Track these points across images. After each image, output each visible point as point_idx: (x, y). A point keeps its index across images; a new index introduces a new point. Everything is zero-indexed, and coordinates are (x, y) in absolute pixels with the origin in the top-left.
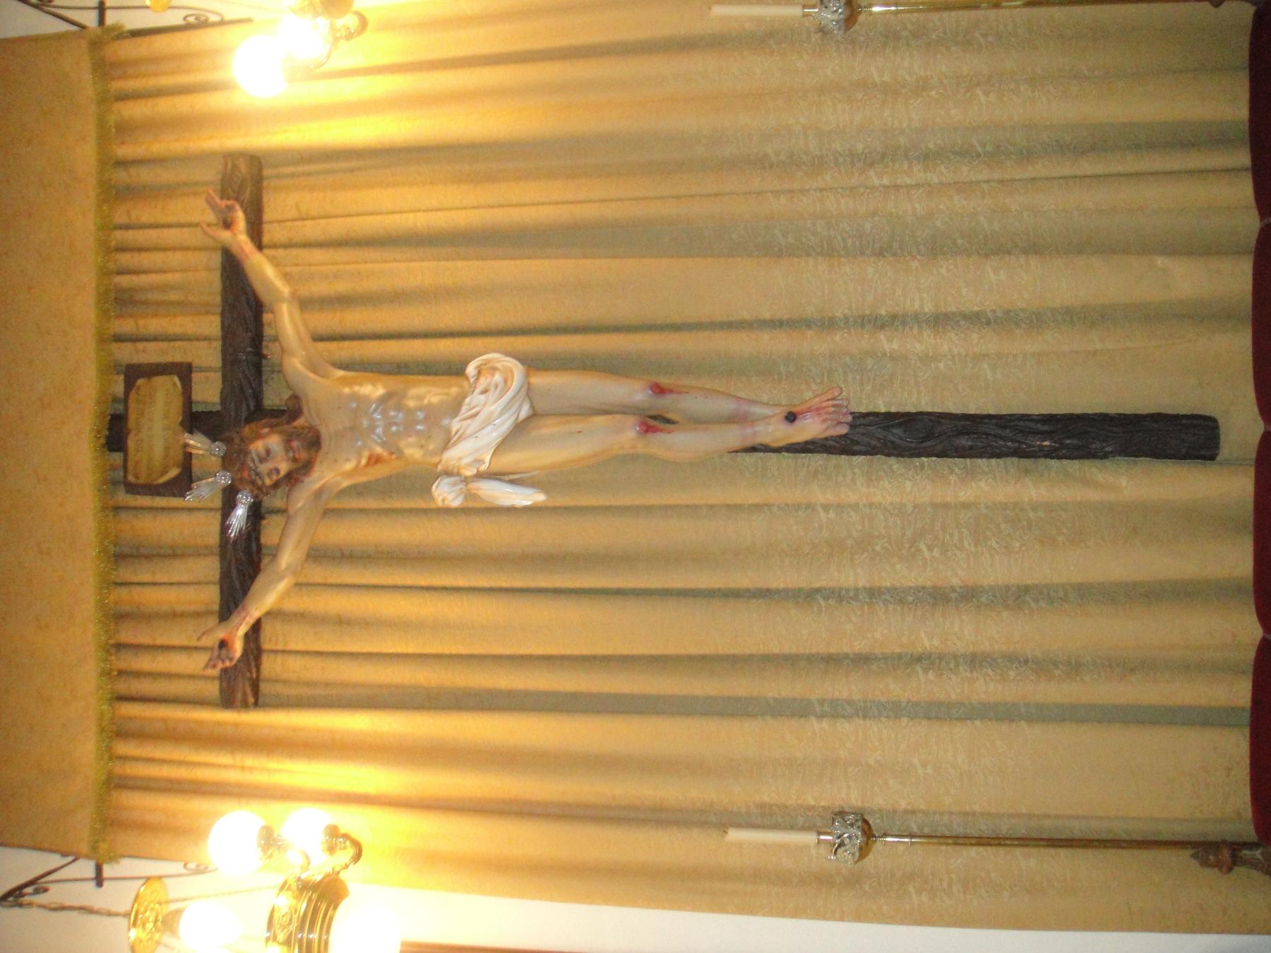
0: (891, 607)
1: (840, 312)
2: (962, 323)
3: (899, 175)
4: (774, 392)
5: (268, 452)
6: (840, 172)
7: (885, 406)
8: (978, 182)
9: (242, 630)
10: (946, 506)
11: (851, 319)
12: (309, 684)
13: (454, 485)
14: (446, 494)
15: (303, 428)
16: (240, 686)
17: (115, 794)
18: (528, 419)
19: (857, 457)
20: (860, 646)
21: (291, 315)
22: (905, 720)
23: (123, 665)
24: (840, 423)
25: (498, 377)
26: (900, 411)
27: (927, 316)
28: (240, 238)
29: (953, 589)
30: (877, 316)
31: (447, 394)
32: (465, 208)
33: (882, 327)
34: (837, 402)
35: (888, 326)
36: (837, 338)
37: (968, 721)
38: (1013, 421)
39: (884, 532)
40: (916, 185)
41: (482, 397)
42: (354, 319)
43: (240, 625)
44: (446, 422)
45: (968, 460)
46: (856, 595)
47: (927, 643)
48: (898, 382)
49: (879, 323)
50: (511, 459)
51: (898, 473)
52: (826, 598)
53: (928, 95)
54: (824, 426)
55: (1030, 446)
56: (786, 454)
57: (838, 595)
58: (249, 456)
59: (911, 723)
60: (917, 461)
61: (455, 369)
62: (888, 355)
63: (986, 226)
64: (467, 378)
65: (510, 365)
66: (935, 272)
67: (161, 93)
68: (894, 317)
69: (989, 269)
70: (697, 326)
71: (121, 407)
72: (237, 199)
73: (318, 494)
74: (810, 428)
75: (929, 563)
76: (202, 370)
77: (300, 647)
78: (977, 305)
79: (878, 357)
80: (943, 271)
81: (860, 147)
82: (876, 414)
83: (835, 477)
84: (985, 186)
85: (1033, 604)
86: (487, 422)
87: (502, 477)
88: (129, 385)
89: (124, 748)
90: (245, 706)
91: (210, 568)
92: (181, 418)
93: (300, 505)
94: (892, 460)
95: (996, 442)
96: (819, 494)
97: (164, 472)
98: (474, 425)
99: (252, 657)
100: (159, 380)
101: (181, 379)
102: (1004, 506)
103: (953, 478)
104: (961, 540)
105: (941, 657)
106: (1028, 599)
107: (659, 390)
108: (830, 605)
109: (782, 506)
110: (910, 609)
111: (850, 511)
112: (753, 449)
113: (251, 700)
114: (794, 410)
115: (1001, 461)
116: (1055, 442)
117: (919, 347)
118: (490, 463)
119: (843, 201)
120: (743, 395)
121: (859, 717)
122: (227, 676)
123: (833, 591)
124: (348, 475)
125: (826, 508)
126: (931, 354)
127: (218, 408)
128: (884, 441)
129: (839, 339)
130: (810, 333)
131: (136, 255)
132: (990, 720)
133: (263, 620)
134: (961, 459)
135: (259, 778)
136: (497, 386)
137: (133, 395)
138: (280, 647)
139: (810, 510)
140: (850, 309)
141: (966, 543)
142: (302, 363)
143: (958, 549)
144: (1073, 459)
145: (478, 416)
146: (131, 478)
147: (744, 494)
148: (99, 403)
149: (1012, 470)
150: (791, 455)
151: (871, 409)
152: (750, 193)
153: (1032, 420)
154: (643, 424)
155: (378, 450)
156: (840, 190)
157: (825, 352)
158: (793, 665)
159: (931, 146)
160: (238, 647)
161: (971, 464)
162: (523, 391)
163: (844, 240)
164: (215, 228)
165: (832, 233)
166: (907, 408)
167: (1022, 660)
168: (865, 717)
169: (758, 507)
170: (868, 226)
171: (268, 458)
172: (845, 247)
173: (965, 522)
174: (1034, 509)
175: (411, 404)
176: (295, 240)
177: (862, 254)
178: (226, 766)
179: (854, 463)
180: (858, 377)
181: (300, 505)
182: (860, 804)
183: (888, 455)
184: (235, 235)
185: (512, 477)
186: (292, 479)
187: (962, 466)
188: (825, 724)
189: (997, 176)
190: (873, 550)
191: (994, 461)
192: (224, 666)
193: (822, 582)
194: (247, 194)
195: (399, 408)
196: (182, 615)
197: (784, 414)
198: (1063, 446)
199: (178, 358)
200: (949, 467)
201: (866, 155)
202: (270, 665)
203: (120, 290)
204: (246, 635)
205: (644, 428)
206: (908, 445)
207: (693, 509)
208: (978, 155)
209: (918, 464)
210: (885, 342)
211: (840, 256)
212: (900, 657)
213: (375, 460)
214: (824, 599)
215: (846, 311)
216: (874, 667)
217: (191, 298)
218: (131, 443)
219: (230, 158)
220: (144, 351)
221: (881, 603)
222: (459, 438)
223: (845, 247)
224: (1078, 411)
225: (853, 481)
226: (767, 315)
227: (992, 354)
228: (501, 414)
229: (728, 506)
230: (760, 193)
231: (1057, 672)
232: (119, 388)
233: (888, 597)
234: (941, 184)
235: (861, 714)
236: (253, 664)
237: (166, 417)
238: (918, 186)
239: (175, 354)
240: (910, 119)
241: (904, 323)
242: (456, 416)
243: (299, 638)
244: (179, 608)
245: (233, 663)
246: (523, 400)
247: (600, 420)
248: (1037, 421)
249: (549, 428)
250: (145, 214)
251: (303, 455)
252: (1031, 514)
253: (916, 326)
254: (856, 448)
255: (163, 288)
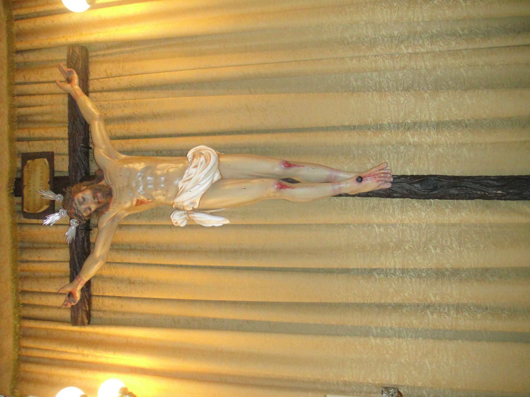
0: (413, 279)
1: (386, 121)
2: (452, 126)
3: (417, 47)
4: (351, 164)
5: (84, 199)
6: (385, 46)
7: (410, 171)
8: (461, 50)
9: (80, 287)
10: (443, 225)
11: (392, 125)
12: (115, 312)
13: (181, 215)
14: (178, 219)
15: (103, 186)
16: (80, 315)
17: (22, 366)
18: (219, 181)
19: (395, 199)
20: (397, 300)
21: (99, 125)
22: (421, 339)
23: (26, 302)
24: (386, 182)
25: (202, 159)
26: (419, 174)
27: (433, 123)
28: (76, 88)
29: (447, 270)
30: (405, 123)
31: (177, 168)
32: (189, 70)
33: (409, 129)
34: (385, 171)
35: (412, 129)
36: (384, 135)
37: (455, 341)
38: (481, 180)
39: (410, 239)
40: (426, 52)
41: (194, 170)
42: (134, 128)
43: (78, 285)
44: (176, 182)
45: (455, 201)
46: (395, 272)
47: (433, 299)
48: (417, 159)
49: (407, 127)
50: (211, 202)
51: (417, 208)
52: (379, 274)
53: (433, 3)
54: (377, 184)
55: (489, 193)
56: (357, 198)
57: (385, 273)
58: (74, 202)
59: (424, 341)
60: (428, 201)
61: (182, 154)
62: (412, 144)
63: (464, 74)
64: (187, 159)
65: (209, 152)
66: (438, 99)
67: (39, 15)
68: (415, 123)
69: (467, 97)
70: (310, 130)
71: (19, 176)
72: (74, 69)
73: (113, 219)
74: (370, 185)
75: (434, 256)
76: (59, 154)
77: (111, 294)
78: (460, 117)
79: (406, 145)
80: (442, 99)
81: (396, 33)
82: (406, 176)
83: (384, 210)
84: (465, 52)
85: (490, 278)
86: (197, 183)
87: (207, 212)
88: (24, 163)
89: (26, 343)
90: (83, 324)
91: (65, 254)
92: (48, 180)
93: (104, 224)
94: (414, 201)
95: (471, 191)
96: (375, 218)
97: (41, 207)
98: (189, 185)
99: (86, 300)
100: (37, 160)
101: (48, 160)
102: (475, 225)
103: (447, 211)
104: (451, 244)
105: (440, 305)
106: (488, 275)
107: (288, 165)
108: (381, 278)
109: (355, 225)
110: (424, 281)
111: (392, 227)
112: (340, 195)
113: (86, 321)
114: (362, 175)
115: (474, 201)
116: (504, 192)
117: (429, 140)
118: (199, 205)
119: (387, 61)
120: (334, 166)
121: (396, 337)
122: (74, 309)
123: (382, 270)
124: (128, 210)
125: (379, 226)
126: (435, 144)
127: (67, 175)
128: (410, 191)
129: (385, 136)
130: (369, 133)
131: (28, 97)
132: (467, 339)
133: (92, 281)
134: (452, 200)
135: (91, 359)
136: (201, 164)
137: (25, 169)
138: (101, 294)
139: (370, 227)
140: (392, 120)
141: (454, 245)
142: (104, 153)
143: (450, 248)
144: (513, 200)
145: (192, 180)
146: (25, 210)
147: (335, 218)
148: (11, 172)
149: (479, 207)
150: (360, 198)
151: (402, 173)
152: (337, 58)
153: (491, 180)
154: (279, 183)
155: (142, 198)
156: (385, 56)
157: (378, 143)
158: (361, 308)
159: (434, 31)
160: (78, 295)
161: (457, 202)
162: (216, 167)
163: (388, 83)
164: (63, 83)
165: (381, 79)
166: (422, 173)
167: (484, 307)
168: (399, 337)
169: (343, 225)
170: (400, 75)
171: (84, 203)
172: (388, 87)
173: (454, 234)
174: (491, 227)
175: (159, 172)
176: (105, 88)
177: (398, 90)
178: (75, 354)
179: (394, 203)
180: (396, 156)
181: (104, 224)
182: (396, 383)
183: (412, 198)
184: (72, 86)
185: (211, 211)
186: (99, 212)
187: (452, 204)
188: (378, 341)
189: (470, 47)
190: (404, 249)
191: (469, 201)
192: (71, 305)
193: (377, 265)
194: (80, 65)
195: (152, 175)
196: (54, 277)
197: (355, 178)
198: (508, 193)
199: (49, 149)
200: (445, 204)
201: (399, 37)
202: (96, 303)
203: (20, 116)
204: (82, 290)
205: (280, 186)
206: (423, 193)
207: (308, 226)
208: (460, 36)
209: (428, 203)
210: (410, 137)
211: (386, 91)
212: (418, 305)
213: (140, 203)
214: (378, 275)
215: (389, 121)
216: (404, 311)
217: (55, 119)
218: (25, 192)
219: (72, 47)
220: (33, 146)
221: (408, 277)
222: (182, 192)
223: (388, 87)
224: (516, 174)
225: (394, 212)
226: (347, 124)
227: (469, 143)
228: (203, 179)
229: (327, 225)
230: (342, 58)
231: (504, 315)
232: (19, 165)
233: (412, 274)
234: (440, 51)
235: (397, 335)
236: (87, 303)
237: (42, 178)
238: (427, 52)
239: (47, 148)
240: (423, 17)
241: (420, 127)
242: (182, 180)
243: (110, 290)
244: (53, 274)
245: (76, 303)
246: (216, 170)
247: (257, 181)
248: (494, 180)
249: (229, 186)
250: (33, 77)
251: (103, 200)
252: (489, 229)
253: (427, 129)
254: (395, 195)
255: (42, 114)
